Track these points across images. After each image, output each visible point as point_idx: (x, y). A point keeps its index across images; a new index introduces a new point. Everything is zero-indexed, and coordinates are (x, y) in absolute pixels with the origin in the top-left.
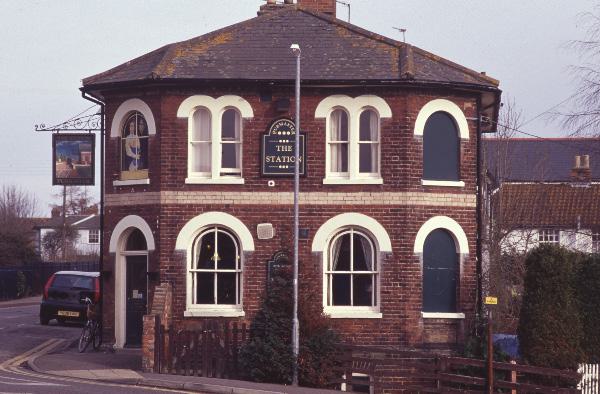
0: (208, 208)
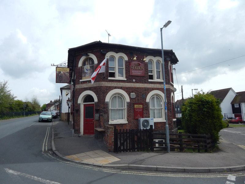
0: (116, 88)
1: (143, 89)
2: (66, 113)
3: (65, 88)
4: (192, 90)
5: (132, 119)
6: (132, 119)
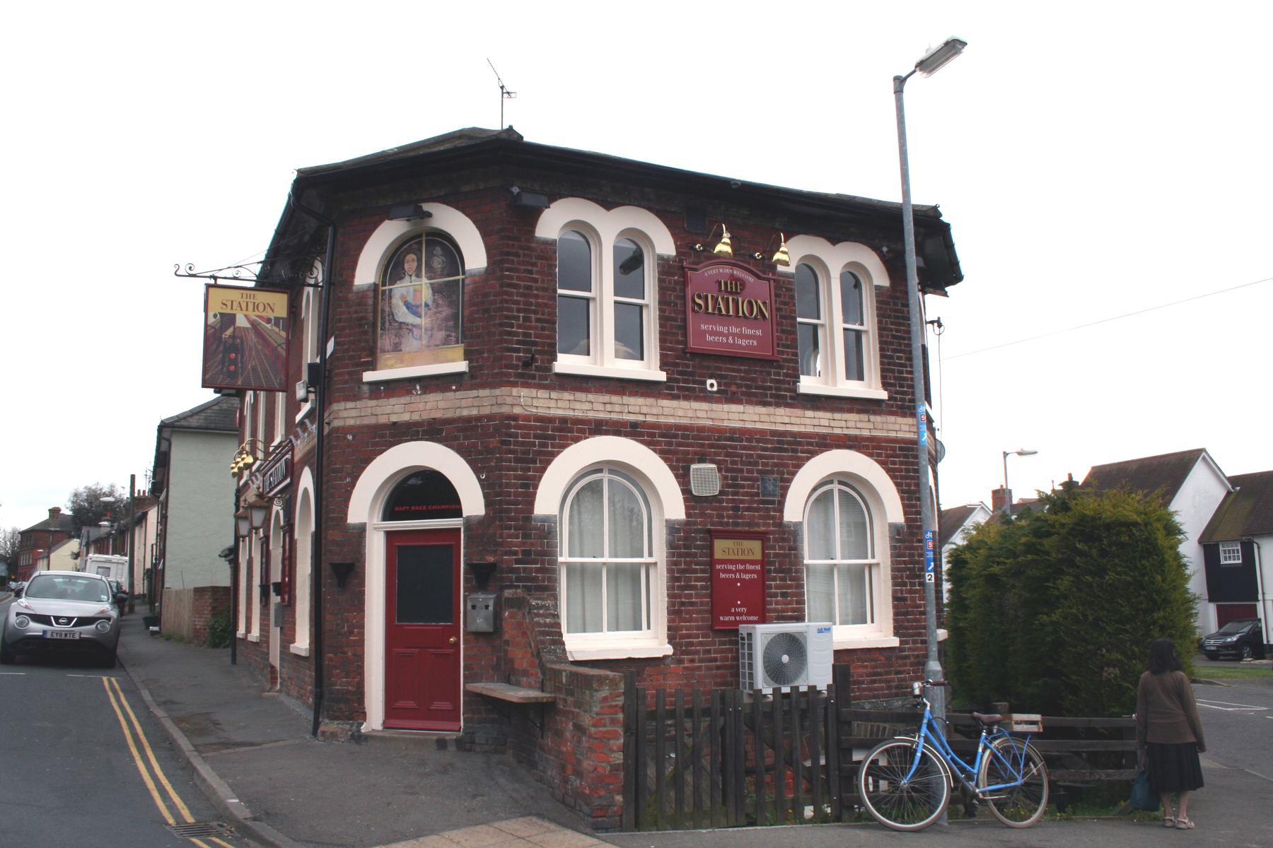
1: (767, 441)
2: (199, 591)
3: (194, 422)
4: (1005, 454)
5: (698, 628)
6: (698, 628)
